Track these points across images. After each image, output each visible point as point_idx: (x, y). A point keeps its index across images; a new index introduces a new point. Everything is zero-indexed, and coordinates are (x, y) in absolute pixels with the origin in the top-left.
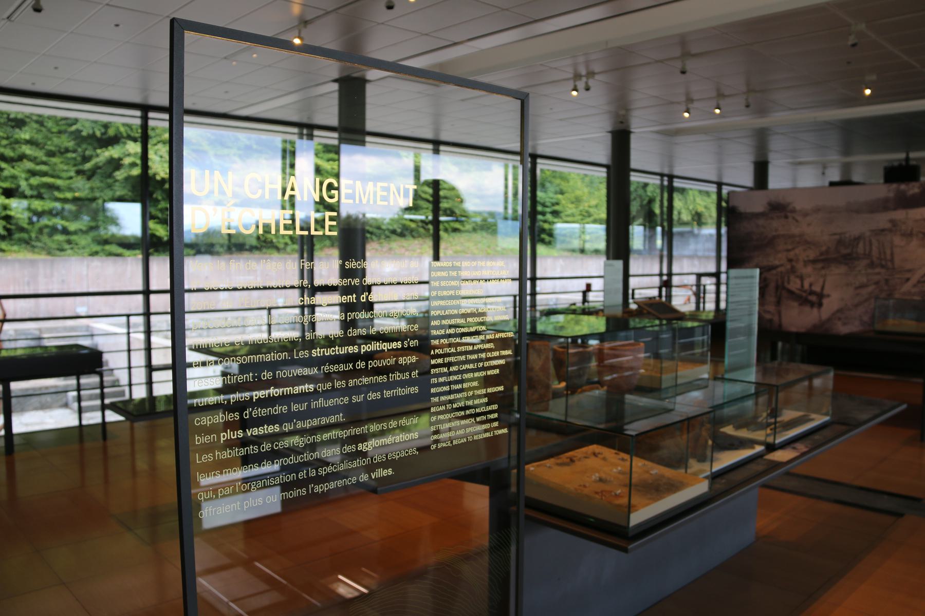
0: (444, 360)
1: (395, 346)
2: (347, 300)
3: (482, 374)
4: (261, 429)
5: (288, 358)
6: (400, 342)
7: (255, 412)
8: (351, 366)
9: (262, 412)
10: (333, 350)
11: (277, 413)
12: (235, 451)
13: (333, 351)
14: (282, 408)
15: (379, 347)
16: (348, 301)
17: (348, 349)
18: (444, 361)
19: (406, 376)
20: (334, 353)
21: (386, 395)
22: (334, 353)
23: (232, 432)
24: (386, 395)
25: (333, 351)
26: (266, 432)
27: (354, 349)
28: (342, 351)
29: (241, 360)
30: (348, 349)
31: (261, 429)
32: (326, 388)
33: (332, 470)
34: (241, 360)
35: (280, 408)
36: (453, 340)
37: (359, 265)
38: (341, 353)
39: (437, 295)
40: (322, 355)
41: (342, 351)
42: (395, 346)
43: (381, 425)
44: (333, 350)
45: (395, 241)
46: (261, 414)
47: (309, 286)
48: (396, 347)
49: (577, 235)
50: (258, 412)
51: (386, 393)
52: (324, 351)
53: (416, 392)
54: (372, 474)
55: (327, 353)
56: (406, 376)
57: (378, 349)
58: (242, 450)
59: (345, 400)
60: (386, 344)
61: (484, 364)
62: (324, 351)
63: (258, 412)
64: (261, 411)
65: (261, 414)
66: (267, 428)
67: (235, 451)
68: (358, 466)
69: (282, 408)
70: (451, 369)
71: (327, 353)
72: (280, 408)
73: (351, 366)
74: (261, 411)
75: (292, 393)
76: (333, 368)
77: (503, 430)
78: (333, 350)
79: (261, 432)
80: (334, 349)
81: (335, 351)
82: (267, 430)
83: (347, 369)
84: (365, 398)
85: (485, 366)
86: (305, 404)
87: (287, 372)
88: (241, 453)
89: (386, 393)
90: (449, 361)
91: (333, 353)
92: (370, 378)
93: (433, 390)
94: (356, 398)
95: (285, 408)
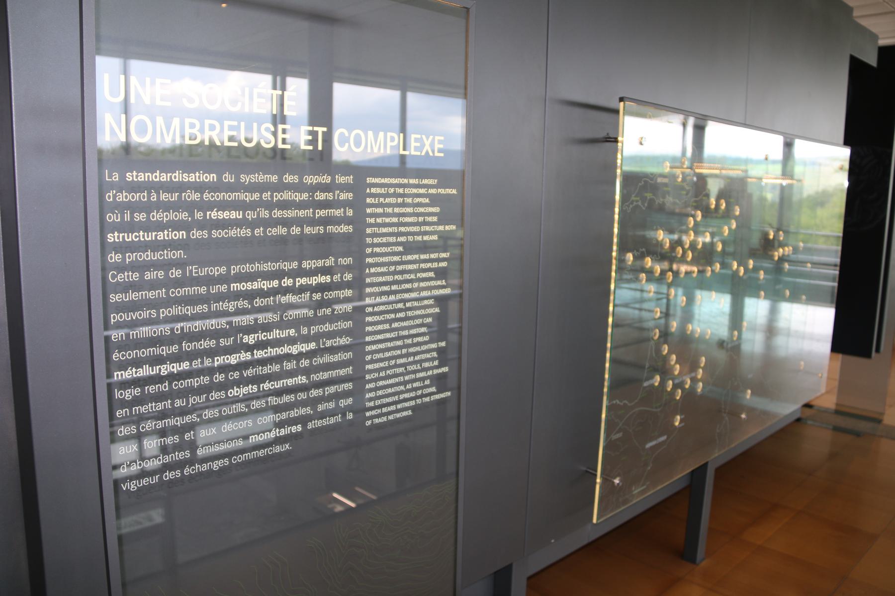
0: (404, 190)
1: (323, 280)
2: (292, 382)
3: (374, 375)
5: (184, 256)
8: (214, 431)
10: (136, 235)
11: (197, 330)
12: (293, 364)
13: (136, 237)
15: (341, 358)
16: (294, 384)
17: (289, 332)
18: (375, 404)
20: (138, 238)
22: (266, 337)
25: (136, 237)
27: (326, 279)
28: (148, 237)
29: (216, 233)
30: (289, 332)
34: (216, 233)
36: (412, 350)
38: (282, 336)
40: (121, 240)
41: (283, 334)
42: (323, 280)
43: (245, 422)
44: (226, 232)
45: (793, 167)
46: (240, 234)
48: (324, 281)
49: (664, 289)
52: (123, 237)
55: (128, 238)
58: (159, 405)
60: (265, 282)
61: (396, 267)
62: (123, 237)
64: (240, 232)
65: (240, 234)
67: (293, 364)
68: (340, 359)
70: (393, 326)
71: (128, 238)
73: (214, 431)
74: (240, 232)
75: (297, 383)
76: (115, 297)
78: (226, 232)
80: (138, 235)
81: (164, 255)
85: (397, 270)
87: (159, 352)
88: (159, 408)
90: (403, 269)
91: (264, 337)
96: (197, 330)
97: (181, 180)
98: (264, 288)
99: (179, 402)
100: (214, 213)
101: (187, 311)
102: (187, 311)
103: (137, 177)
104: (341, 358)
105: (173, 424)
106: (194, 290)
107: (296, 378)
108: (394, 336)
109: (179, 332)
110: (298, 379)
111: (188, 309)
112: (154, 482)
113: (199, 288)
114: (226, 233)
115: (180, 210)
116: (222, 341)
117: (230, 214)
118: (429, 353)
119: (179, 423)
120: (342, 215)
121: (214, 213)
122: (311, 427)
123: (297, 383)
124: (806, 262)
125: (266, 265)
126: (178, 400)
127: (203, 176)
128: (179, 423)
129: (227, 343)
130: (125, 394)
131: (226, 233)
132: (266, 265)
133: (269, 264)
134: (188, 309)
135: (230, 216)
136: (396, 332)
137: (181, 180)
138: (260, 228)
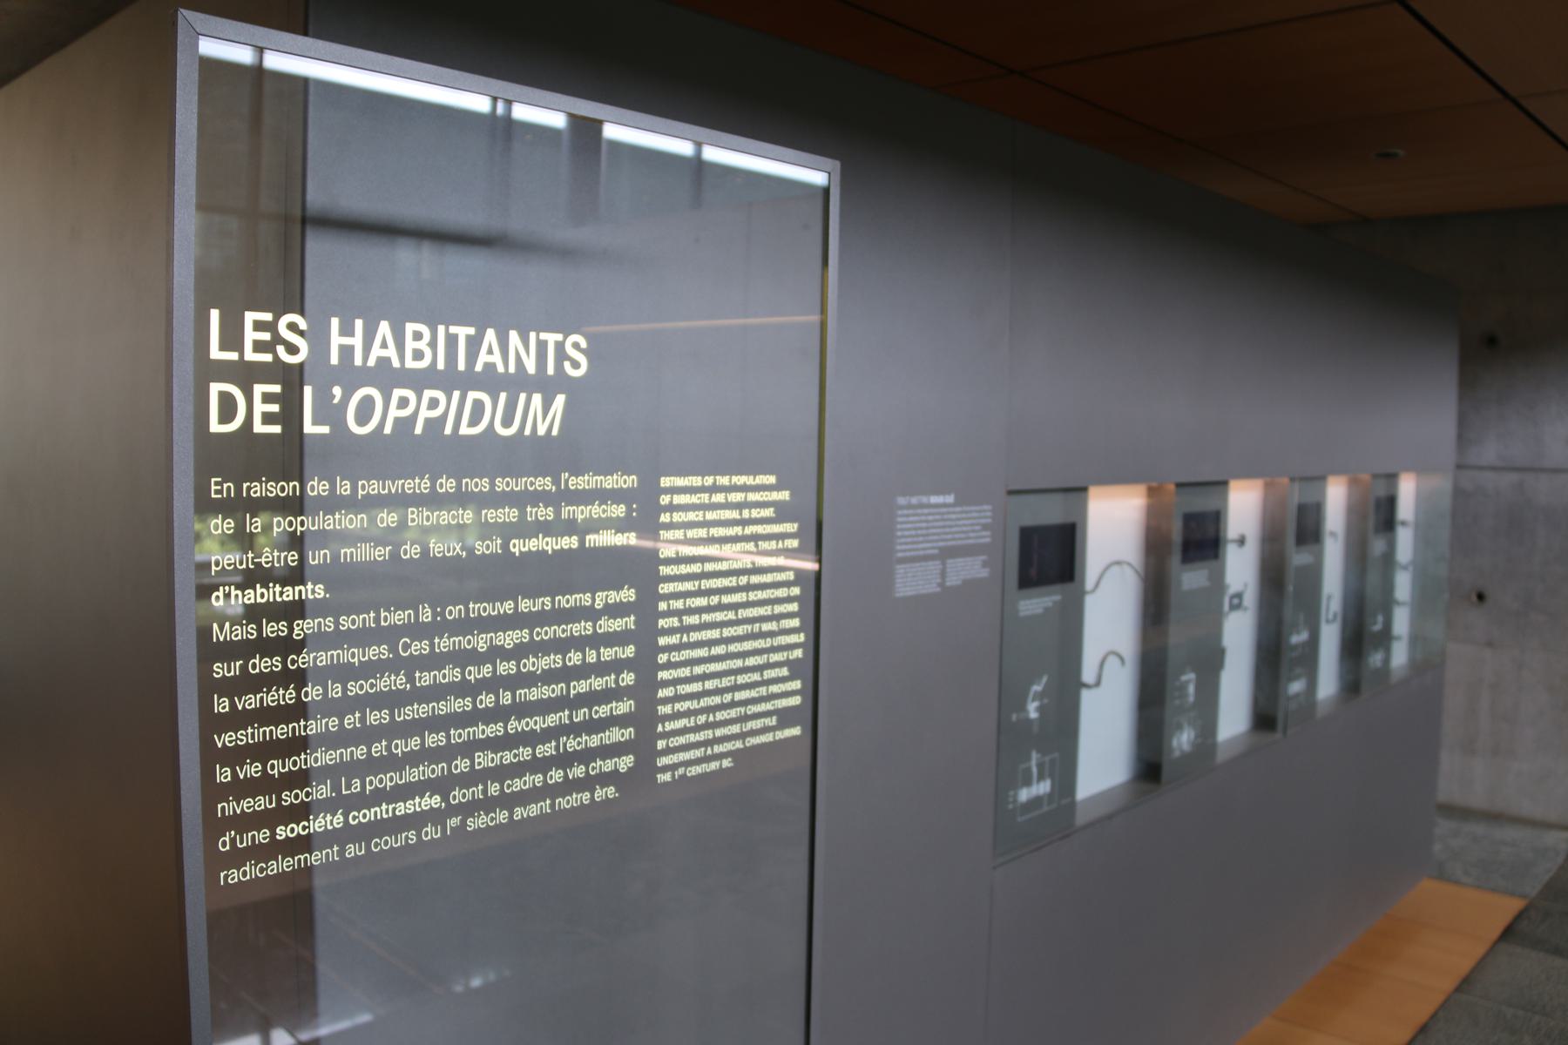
4: (410, 804)
6: (502, 725)
7: (273, 696)
9: (420, 711)
11: (248, 877)
14: (534, 780)
15: (424, 775)
19: (405, 713)
21: (439, 648)
22: (357, 820)
23: (936, 551)
24: (439, 648)
26: (418, 809)
31: (410, 804)
32: (409, 749)
33: (487, 822)
35: (531, 778)
37: (492, 820)
39: (669, 660)
40: (390, 815)
46: (284, 700)
47: (443, 804)
50: (279, 695)
51: (439, 643)
53: (524, 640)
54: (568, 770)
56: (405, 713)
57: (385, 816)
59: (300, 661)
63: (279, 695)
64: (395, 681)
66: (420, 803)
69: (534, 780)
72: (531, 778)
74: (395, 681)
75: (379, 817)
77: (722, 729)
79: (410, 809)
82: (420, 806)
83: (451, 554)
84: (244, 668)
86: (238, 664)
89: (439, 643)
92: (338, 752)
93: (662, 641)
94: (223, 669)
95: (334, 721)
96: (248, 877)
97: (264, 495)
98: (355, 663)
99: (262, 802)
100: (426, 483)
101: (353, 657)
102: (353, 657)
103: (281, 593)
104: (424, 775)
105: (372, 559)
106: (332, 655)
107: (377, 809)
108: (729, 684)
109: (228, 848)
110: (381, 811)
111: (353, 654)
112: (250, 835)
113: (273, 728)
114: (372, 686)
115: (244, 622)
116: (218, 667)
117: (255, 803)
118: (754, 688)
119: (276, 771)
120: (358, 725)
121: (426, 483)
122: (417, 778)
123: (379, 817)
124: (820, 561)
125: (409, 710)
126: (262, 798)
127: (345, 519)
128: (276, 771)
129: (229, 671)
130: (505, 639)
131: (372, 686)
132: (409, 710)
133: (416, 706)
134: (353, 654)
135: (254, 806)
136: (733, 678)
137: (264, 495)
138: (353, 714)
